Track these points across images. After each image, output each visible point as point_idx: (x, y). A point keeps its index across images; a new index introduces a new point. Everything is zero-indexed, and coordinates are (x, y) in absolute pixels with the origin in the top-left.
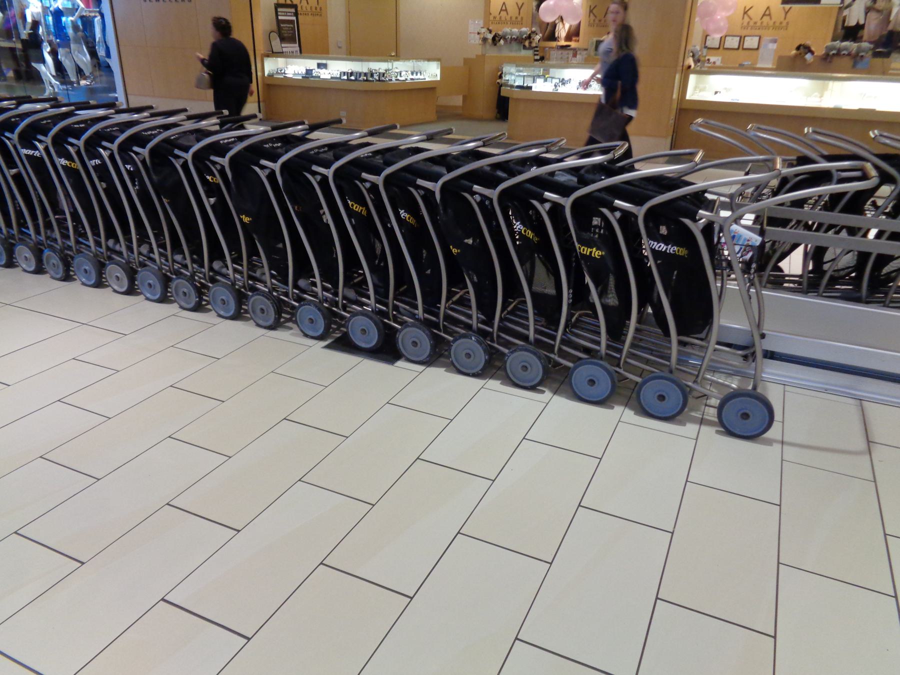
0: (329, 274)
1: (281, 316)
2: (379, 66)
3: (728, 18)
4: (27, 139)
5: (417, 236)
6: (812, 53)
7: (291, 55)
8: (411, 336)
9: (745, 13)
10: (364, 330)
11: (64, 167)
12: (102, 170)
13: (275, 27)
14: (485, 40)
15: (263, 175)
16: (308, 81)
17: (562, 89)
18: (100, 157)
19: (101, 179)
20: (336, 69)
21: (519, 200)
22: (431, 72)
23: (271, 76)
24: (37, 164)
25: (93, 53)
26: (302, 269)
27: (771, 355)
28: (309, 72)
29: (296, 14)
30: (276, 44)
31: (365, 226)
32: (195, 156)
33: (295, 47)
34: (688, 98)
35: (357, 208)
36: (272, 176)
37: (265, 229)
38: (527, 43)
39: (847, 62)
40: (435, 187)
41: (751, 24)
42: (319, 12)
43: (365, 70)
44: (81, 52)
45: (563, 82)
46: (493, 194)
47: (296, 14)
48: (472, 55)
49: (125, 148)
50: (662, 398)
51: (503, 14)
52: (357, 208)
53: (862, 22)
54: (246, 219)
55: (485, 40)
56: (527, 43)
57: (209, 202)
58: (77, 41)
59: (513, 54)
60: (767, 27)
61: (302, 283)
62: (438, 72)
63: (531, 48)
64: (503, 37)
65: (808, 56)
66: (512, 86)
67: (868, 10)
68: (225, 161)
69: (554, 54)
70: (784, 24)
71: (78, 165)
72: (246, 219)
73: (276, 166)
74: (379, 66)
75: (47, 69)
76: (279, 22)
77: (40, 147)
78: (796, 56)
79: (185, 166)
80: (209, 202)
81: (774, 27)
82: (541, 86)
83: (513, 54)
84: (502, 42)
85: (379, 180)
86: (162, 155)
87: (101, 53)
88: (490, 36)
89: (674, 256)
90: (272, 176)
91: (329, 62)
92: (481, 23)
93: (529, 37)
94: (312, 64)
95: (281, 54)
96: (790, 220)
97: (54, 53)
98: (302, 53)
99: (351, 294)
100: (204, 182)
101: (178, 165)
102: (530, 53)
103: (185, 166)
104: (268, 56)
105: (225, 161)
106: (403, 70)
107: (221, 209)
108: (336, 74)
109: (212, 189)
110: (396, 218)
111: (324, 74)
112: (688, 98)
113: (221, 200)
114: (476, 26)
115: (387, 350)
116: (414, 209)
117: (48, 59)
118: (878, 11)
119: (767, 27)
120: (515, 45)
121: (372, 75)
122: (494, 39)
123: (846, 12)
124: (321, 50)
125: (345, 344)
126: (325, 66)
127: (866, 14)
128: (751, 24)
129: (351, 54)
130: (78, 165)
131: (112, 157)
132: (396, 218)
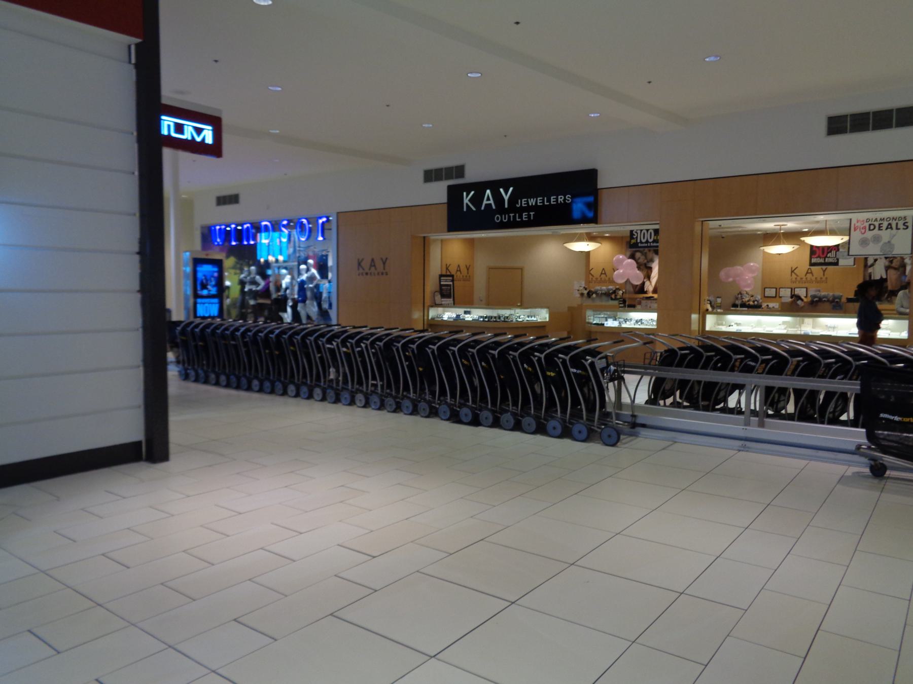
0: (453, 396)
1: (433, 413)
2: (505, 312)
3: (754, 278)
4: (329, 341)
5: (488, 372)
6: (802, 300)
7: (448, 306)
8: (486, 415)
9: (792, 272)
10: (465, 413)
11: (345, 352)
12: (361, 353)
13: (438, 289)
14: (582, 294)
15: (429, 351)
16: (457, 326)
17: (624, 326)
18: (361, 347)
19: (360, 356)
20: (475, 314)
21: (526, 356)
22: (542, 315)
23: (433, 319)
24: (332, 351)
25: (320, 305)
26: (443, 392)
27: (644, 426)
28: (458, 316)
29: (453, 281)
30: (438, 297)
31: (469, 371)
32: (403, 345)
33: (450, 301)
34: (707, 328)
35: (466, 362)
36: (433, 352)
37: (428, 375)
38: (613, 296)
39: (827, 306)
40: (496, 353)
41: (799, 279)
42: (468, 279)
43: (495, 315)
44: (313, 305)
45: (626, 320)
46: (516, 354)
47: (453, 281)
48: (575, 304)
49: (373, 343)
50: (580, 432)
51: (603, 276)
52: (466, 362)
53: (884, 277)
54: (421, 369)
55: (582, 294)
56: (613, 296)
57: (405, 364)
58: (312, 299)
59: (604, 303)
60: (811, 282)
61: (442, 398)
62: (547, 316)
63: (616, 299)
64: (596, 292)
65: (799, 302)
66: (591, 324)
67: (887, 268)
68: (414, 346)
69: (644, 302)
70: (824, 279)
71: (350, 351)
72: (421, 369)
73: (435, 348)
74: (505, 312)
75: (287, 316)
76: (441, 286)
77: (335, 343)
78: (792, 303)
79: (397, 350)
80: (405, 364)
81: (817, 282)
82: (611, 323)
83: (604, 303)
84: (594, 295)
85: (474, 351)
86: (389, 345)
87: (325, 306)
88: (585, 292)
89: (580, 374)
90: (433, 352)
91: (473, 310)
92: (583, 284)
93: (614, 292)
94: (460, 311)
95: (440, 305)
96: (600, 353)
97: (294, 308)
98: (455, 304)
99: (462, 401)
100: (405, 355)
101: (394, 349)
102: (616, 303)
103: (397, 350)
104: (432, 306)
105: (414, 346)
106: (521, 315)
107: (411, 367)
108: (476, 317)
109: (407, 358)
110: (481, 365)
111: (468, 318)
112: (707, 328)
113: (411, 363)
114: (579, 285)
115: (475, 422)
116: (488, 362)
117: (289, 310)
118: (895, 269)
119: (811, 282)
120: (604, 298)
121: (499, 317)
122: (588, 293)
123: (870, 270)
124: (468, 302)
125: (459, 422)
126: (469, 313)
127: (886, 271)
128: (799, 279)
129: (488, 305)
130: (350, 351)
131: (366, 347)
132: (481, 365)
